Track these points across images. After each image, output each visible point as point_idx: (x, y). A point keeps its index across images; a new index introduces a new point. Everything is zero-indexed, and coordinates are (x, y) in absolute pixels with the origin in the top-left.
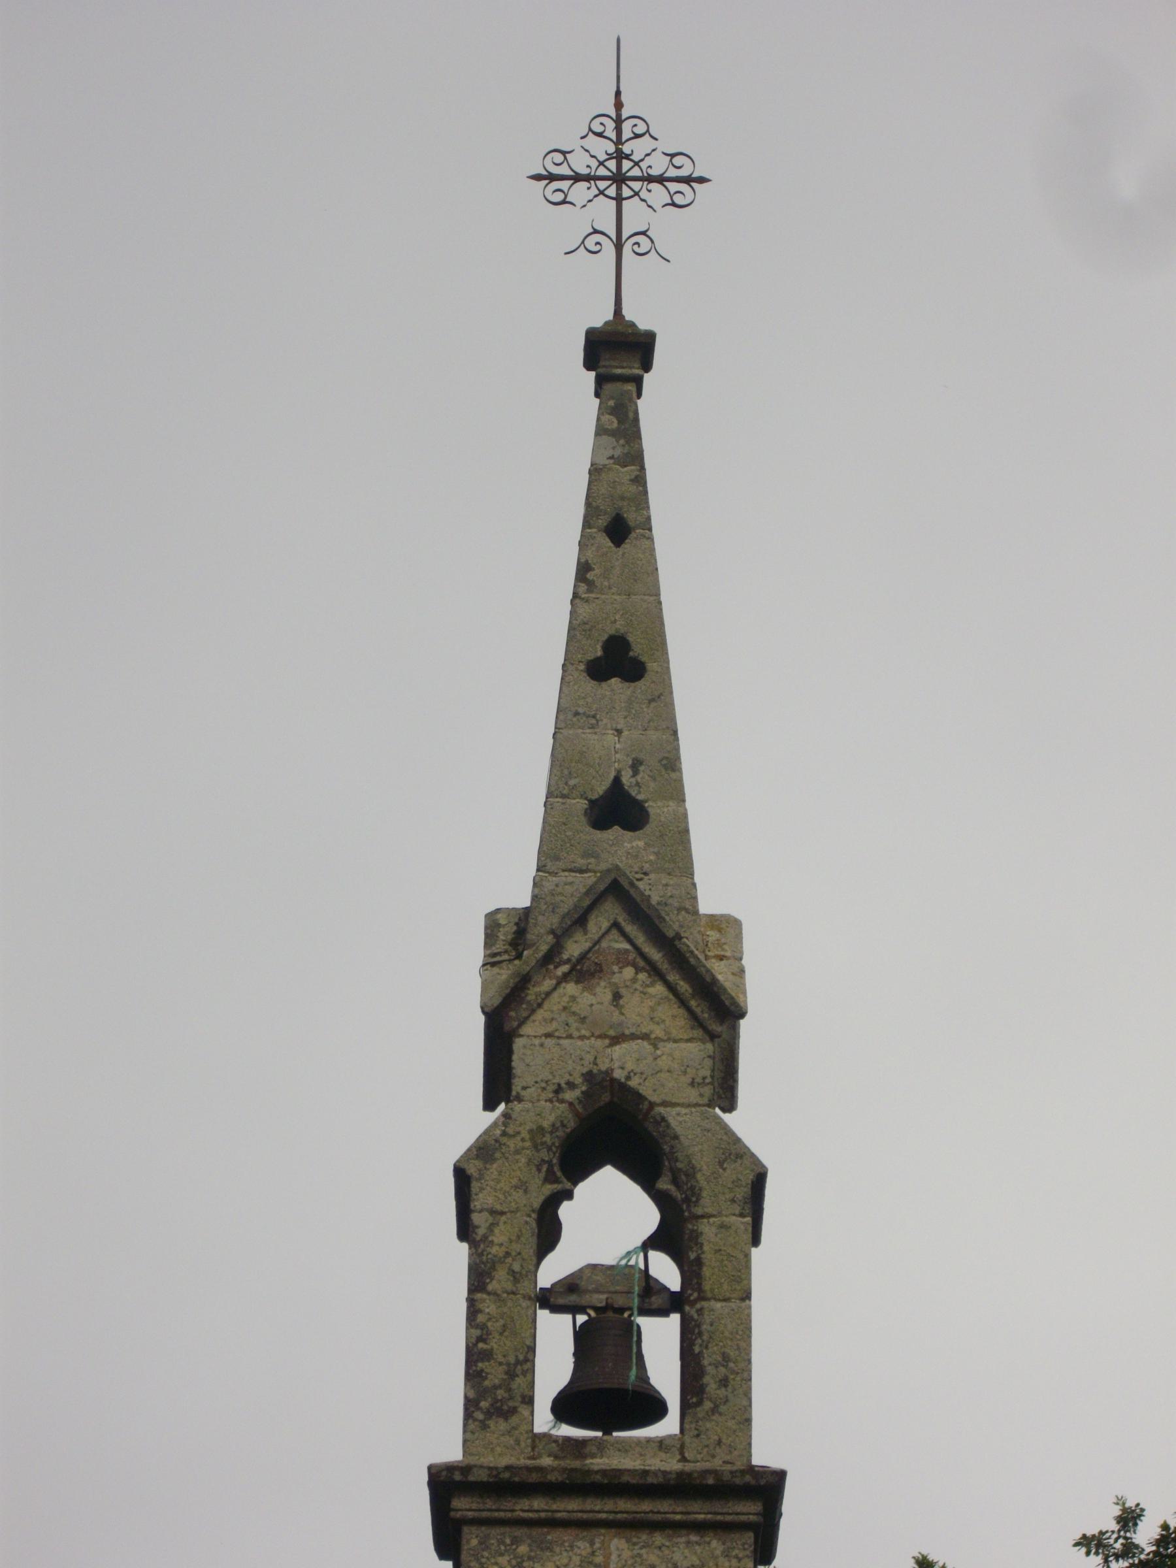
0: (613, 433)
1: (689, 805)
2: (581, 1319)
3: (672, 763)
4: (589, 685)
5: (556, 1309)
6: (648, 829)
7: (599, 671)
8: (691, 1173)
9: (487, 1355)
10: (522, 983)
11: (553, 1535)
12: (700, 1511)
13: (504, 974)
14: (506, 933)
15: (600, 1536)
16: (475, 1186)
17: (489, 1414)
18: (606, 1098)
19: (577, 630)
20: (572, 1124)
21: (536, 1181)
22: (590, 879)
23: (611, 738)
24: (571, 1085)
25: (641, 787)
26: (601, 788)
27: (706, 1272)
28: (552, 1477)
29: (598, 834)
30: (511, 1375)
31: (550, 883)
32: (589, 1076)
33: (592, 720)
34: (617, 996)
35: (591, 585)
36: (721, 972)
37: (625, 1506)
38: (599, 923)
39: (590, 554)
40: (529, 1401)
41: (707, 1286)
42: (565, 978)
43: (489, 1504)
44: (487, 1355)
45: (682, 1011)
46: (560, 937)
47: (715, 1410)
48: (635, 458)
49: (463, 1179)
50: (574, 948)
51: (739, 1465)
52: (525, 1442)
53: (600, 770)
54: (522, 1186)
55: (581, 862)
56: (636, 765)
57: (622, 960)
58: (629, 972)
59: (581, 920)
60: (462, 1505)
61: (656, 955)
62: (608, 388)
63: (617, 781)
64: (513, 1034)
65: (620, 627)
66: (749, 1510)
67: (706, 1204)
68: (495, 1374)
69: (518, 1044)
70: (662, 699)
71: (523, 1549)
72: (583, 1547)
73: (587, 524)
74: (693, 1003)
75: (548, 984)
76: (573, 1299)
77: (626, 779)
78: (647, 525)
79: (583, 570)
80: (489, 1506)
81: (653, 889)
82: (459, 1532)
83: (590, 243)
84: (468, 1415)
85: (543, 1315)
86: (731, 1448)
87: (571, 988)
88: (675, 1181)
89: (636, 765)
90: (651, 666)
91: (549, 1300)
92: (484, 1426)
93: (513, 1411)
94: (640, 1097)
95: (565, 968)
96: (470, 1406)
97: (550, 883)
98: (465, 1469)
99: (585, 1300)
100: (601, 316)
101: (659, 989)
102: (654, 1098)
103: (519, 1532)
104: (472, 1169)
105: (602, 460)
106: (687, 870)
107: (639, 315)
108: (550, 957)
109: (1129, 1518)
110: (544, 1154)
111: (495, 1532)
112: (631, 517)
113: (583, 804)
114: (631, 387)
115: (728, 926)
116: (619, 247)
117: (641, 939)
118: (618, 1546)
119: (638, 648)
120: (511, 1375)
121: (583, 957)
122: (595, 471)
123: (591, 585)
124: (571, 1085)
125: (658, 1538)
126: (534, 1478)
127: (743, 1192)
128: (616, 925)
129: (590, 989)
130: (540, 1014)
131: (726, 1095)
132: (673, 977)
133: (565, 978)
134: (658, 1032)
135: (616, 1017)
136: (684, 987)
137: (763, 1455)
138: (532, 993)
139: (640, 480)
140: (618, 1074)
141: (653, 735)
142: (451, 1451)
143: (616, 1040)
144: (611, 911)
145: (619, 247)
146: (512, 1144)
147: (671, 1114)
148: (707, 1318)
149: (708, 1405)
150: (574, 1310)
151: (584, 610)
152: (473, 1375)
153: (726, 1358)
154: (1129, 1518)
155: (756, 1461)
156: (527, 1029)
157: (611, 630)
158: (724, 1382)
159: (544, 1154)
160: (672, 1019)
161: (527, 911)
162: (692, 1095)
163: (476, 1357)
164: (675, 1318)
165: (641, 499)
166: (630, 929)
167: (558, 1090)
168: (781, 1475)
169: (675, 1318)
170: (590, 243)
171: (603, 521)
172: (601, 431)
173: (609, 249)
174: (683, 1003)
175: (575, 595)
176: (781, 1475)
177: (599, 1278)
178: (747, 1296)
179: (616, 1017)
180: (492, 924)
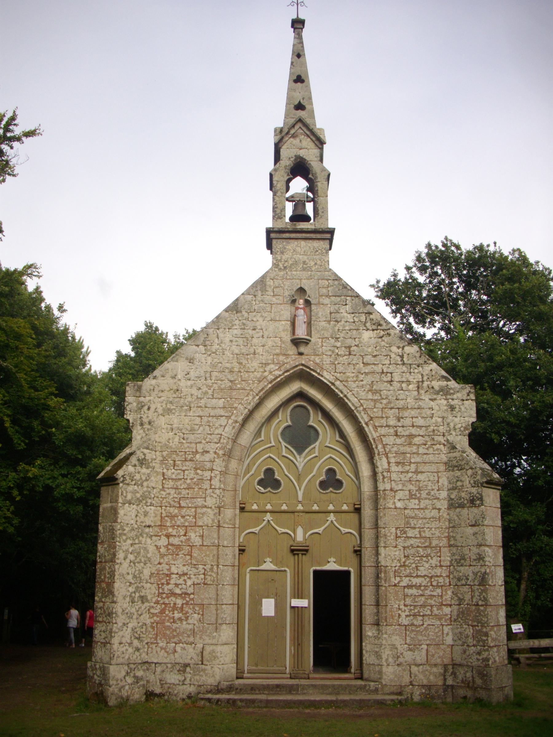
0: (297, 38)
1: (314, 106)
2: (294, 203)
3: (310, 98)
4: (294, 84)
5: (290, 201)
6: (306, 110)
7: (296, 81)
8: (316, 174)
9: (277, 208)
10: (281, 140)
11: (290, 241)
12: (318, 236)
13: (278, 137)
14: (278, 131)
15: (299, 241)
16: (274, 176)
17: (277, 219)
18: (299, 160)
19: (291, 74)
20: (292, 165)
21: (286, 175)
22: (294, 119)
23: (298, 94)
24: (292, 157)
25: (304, 103)
26: (296, 103)
27: (319, 192)
28: (290, 230)
29: (296, 111)
30: (281, 211)
31: (287, 120)
32: (296, 156)
33: (295, 90)
34: (301, 141)
35: (294, 66)
36: (321, 136)
37: (304, 235)
38: (297, 127)
39: (293, 60)
40: (285, 216)
41: (319, 194)
42: (291, 137)
43: (278, 235)
44: (277, 208)
45: (313, 144)
46: (290, 129)
47: (321, 217)
48: (302, 43)
49: (271, 175)
50: (292, 132)
51: (326, 227)
52: (284, 224)
53: (264, 318)
54: (283, 176)
55: (293, 116)
56: (303, 99)
57: (301, 134)
58: (303, 136)
59: (293, 126)
60: (273, 235)
61: (308, 133)
62: (296, 30)
63: (300, 102)
64: (280, 148)
65: (299, 73)
66: (328, 236)
67: (319, 179)
68: (278, 211)
69: (282, 150)
70: (308, 87)
71: (284, 243)
72: (296, 243)
73: (293, 55)
74: (316, 142)
75: (287, 138)
76: (292, 199)
77: (302, 101)
78: (304, 55)
79: (292, 63)
80: (278, 235)
81: (308, 121)
82: (272, 241)
83: (292, 4)
84: (273, 219)
85: (287, 203)
86: (324, 224)
87: (292, 139)
88: (313, 175)
89: (303, 99)
90: (306, 80)
91: (287, 200)
92: (276, 221)
93: (282, 218)
94: (305, 160)
95: (290, 136)
96: (274, 217)
97: (287, 120)
98: (273, 228)
99: (295, 199)
100: (295, 17)
101: (309, 139)
102: (308, 159)
103: (284, 240)
104: (273, 173)
105: (295, 43)
106: (314, 118)
107: (301, 17)
108: (287, 133)
109: (378, 282)
110: (287, 170)
111: (279, 240)
112: (301, 53)
113: (293, 106)
114: (301, 30)
115: (321, 130)
116: (297, 4)
117: (305, 130)
118: (303, 243)
119: (303, 77)
120: (281, 211)
121: (294, 133)
122: (294, 45)
123: (294, 66)
124: (292, 157)
125: (311, 241)
126: (286, 230)
127: (326, 177)
128: (300, 128)
129: (295, 140)
130: (286, 144)
131: (321, 160)
132: (312, 137)
133: (291, 137)
134: (309, 147)
135: (300, 145)
136: (314, 139)
137: (330, 225)
138: (284, 140)
139: (303, 47)
140: (301, 155)
141: (307, 93)
142: (270, 225)
143: (301, 149)
144: (299, 125)
145: (297, 4)
146: (281, 168)
147: (312, 163)
148: (319, 200)
149: (320, 216)
150: (292, 201)
151: (293, 70)
152: (274, 211)
153: (323, 208)
154: (378, 282)
155: (329, 227)
156: (283, 147)
157: (297, 74)
158: (323, 212)
159: (287, 170)
160: (312, 145)
161: (282, 128)
162: (316, 159)
163: (274, 208)
164: (312, 203)
165: (303, 50)
166: (303, 128)
167: (290, 158)
168: (334, 229)
169: (312, 203)
170: (292, 4)
171: (296, 54)
172: (295, 38)
173: (296, 5)
174: (314, 142)
175: (291, 68)
176: (334, 229)
177: (298, 195)
178: (327, 196)
179: (300, 145)
180: (276, 130)
